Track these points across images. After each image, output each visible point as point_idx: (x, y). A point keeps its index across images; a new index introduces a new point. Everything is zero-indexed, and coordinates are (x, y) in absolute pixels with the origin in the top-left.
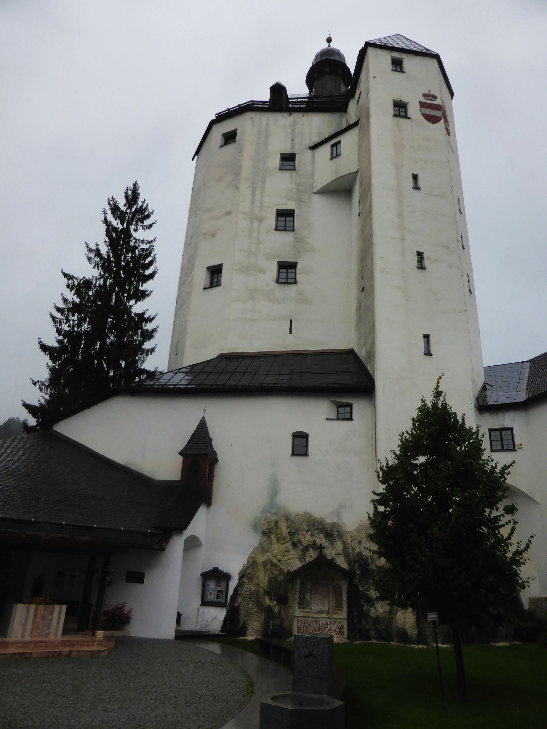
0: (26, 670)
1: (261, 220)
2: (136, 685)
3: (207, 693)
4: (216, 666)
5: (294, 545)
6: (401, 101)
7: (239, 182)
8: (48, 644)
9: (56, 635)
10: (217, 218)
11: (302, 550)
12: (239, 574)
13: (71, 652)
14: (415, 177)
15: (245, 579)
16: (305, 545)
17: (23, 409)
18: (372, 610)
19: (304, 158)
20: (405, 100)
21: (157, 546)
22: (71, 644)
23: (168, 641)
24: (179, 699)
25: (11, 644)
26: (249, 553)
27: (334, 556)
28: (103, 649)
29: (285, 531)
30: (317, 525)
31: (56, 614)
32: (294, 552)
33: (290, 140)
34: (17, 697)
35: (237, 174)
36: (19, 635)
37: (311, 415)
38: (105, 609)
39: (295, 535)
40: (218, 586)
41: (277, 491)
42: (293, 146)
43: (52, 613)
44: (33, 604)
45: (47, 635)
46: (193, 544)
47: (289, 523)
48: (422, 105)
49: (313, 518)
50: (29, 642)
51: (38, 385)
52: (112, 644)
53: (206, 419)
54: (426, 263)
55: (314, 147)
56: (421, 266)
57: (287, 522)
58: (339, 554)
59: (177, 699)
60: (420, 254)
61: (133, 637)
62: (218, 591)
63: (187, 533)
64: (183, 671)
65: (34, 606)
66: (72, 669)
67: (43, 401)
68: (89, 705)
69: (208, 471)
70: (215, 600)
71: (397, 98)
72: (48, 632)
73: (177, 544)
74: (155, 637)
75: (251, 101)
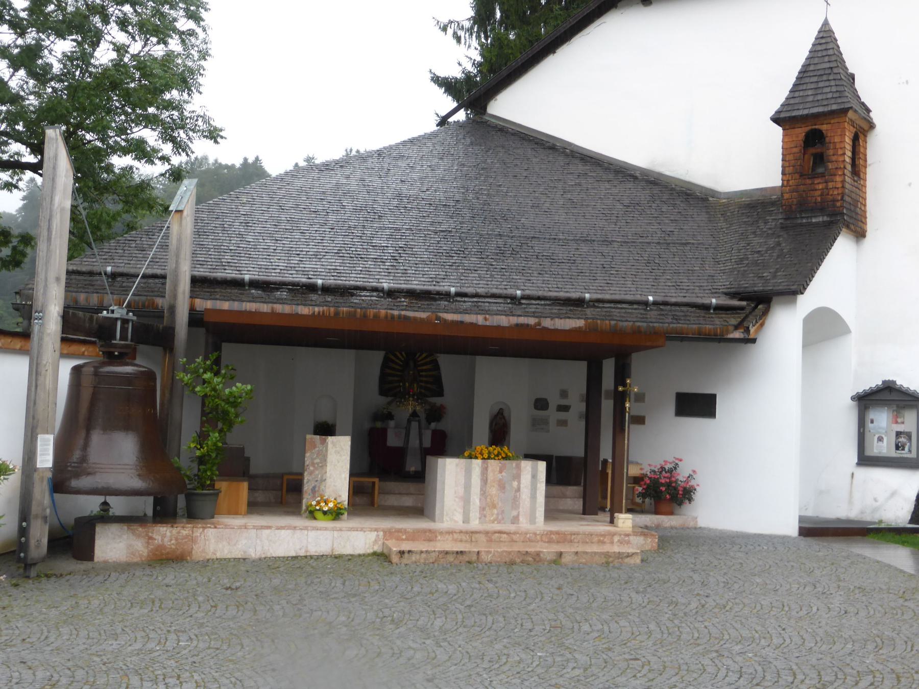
0: (464, 584)
2: (696, 635)
3: (880, 667)
4: (901, 601)
8: (515, 537)
9: (532, 520)
13: (560, 554)
17: (435, 87)
21: (737, 335)
22: (564, 538)
23: (784, 539)
24: (800, 677)
25: (441, 533)
28: (631, 551)
31: (526, 478)
34: (428, 642)
36: (459, 517)
38: (633, 471)
40: (897, 422)
43: (517, 477)
44: (476, 458)
45: (515, 520)
46: (824, 328)
50: (476, 532)
51: (450, 31)
52: (650, 543)
53: (834, 26)
59: (795, 675)
61: (704, 528)
62: (898, 434)
63: (808, 302)
64: (815, 609)
65: (479, 461)
66: (559, 588)
67: (470, 68)
68: (577, 672)
69: (849, 154)
70: (893, 453)
72: (514, 513)
73: (785, 327)
74: (97, 537)
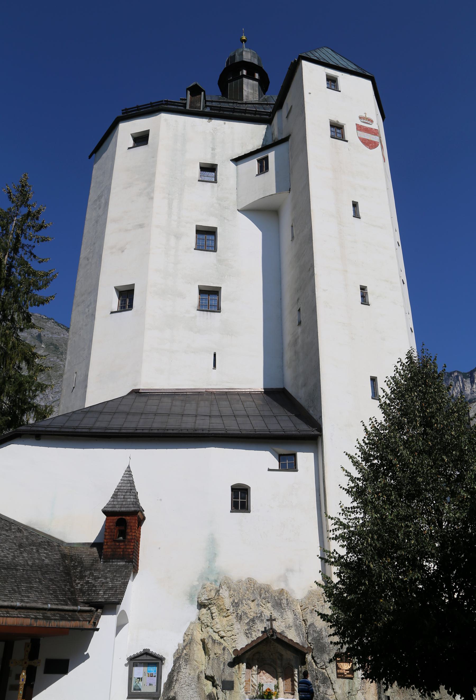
1: (178, 237)
5: (240, 618)
6: (338, 121)
7: (153, 191)
10: (126, 230)
11: (248, 624)
12: (174, 656)
14: (355, 205)
15: (182, 661)
16: (252, 617)
18: (330, 691)
19: (227, 170)
20: (341, 121)
26: (184, 629)
27: (284, 629)
29: (227, 602)
30: (262, 592)
32: (239, 626)
33: (211, 149)
35: (151, 182)
37: (253, 465)
39: (239, 605)
41: (215, 554)
42: (213, 156)
47: (232, 592)
48: (359, 128)
49: (258, 585)
54: (370, 298)
55: (237, 160)
56: (364, 300)
57: (230, 591)
58: (289, 627)
60: (363, 289)
71: (335, 119)
75: (165, 101)
